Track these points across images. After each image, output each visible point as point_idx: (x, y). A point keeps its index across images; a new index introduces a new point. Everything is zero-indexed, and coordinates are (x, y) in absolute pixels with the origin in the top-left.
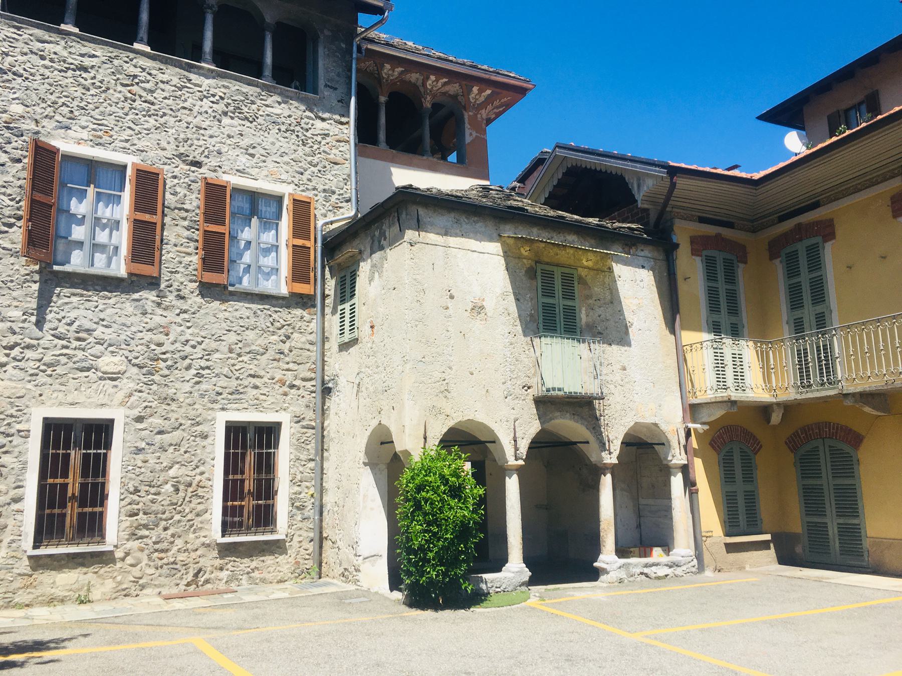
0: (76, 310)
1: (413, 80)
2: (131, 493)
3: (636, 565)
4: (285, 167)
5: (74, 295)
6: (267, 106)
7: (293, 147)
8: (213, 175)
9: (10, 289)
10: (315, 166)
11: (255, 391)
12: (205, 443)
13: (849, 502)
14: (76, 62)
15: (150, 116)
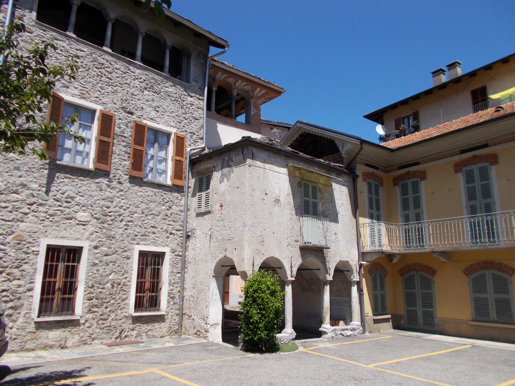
0: (67, 186)
1: (230, 81)
2: (90, 288)
3: (338, 330)
4: (173, 119)
5: (66, 178)
6: (166, 87)
7: (177, 109)
8: (138, 120)
9: (32, 172)
10: (186, 120)
11: (153, 235)
12: (128, 262)
13: (428, 301)
14: (74, 53)
15: (109, 86)
